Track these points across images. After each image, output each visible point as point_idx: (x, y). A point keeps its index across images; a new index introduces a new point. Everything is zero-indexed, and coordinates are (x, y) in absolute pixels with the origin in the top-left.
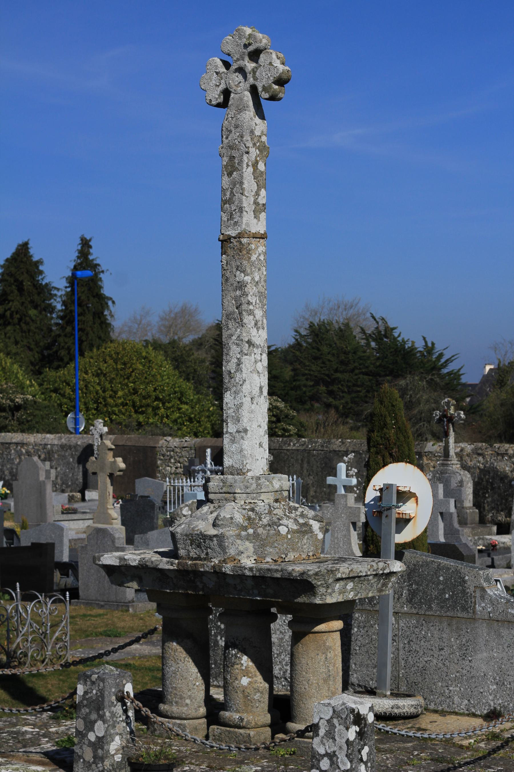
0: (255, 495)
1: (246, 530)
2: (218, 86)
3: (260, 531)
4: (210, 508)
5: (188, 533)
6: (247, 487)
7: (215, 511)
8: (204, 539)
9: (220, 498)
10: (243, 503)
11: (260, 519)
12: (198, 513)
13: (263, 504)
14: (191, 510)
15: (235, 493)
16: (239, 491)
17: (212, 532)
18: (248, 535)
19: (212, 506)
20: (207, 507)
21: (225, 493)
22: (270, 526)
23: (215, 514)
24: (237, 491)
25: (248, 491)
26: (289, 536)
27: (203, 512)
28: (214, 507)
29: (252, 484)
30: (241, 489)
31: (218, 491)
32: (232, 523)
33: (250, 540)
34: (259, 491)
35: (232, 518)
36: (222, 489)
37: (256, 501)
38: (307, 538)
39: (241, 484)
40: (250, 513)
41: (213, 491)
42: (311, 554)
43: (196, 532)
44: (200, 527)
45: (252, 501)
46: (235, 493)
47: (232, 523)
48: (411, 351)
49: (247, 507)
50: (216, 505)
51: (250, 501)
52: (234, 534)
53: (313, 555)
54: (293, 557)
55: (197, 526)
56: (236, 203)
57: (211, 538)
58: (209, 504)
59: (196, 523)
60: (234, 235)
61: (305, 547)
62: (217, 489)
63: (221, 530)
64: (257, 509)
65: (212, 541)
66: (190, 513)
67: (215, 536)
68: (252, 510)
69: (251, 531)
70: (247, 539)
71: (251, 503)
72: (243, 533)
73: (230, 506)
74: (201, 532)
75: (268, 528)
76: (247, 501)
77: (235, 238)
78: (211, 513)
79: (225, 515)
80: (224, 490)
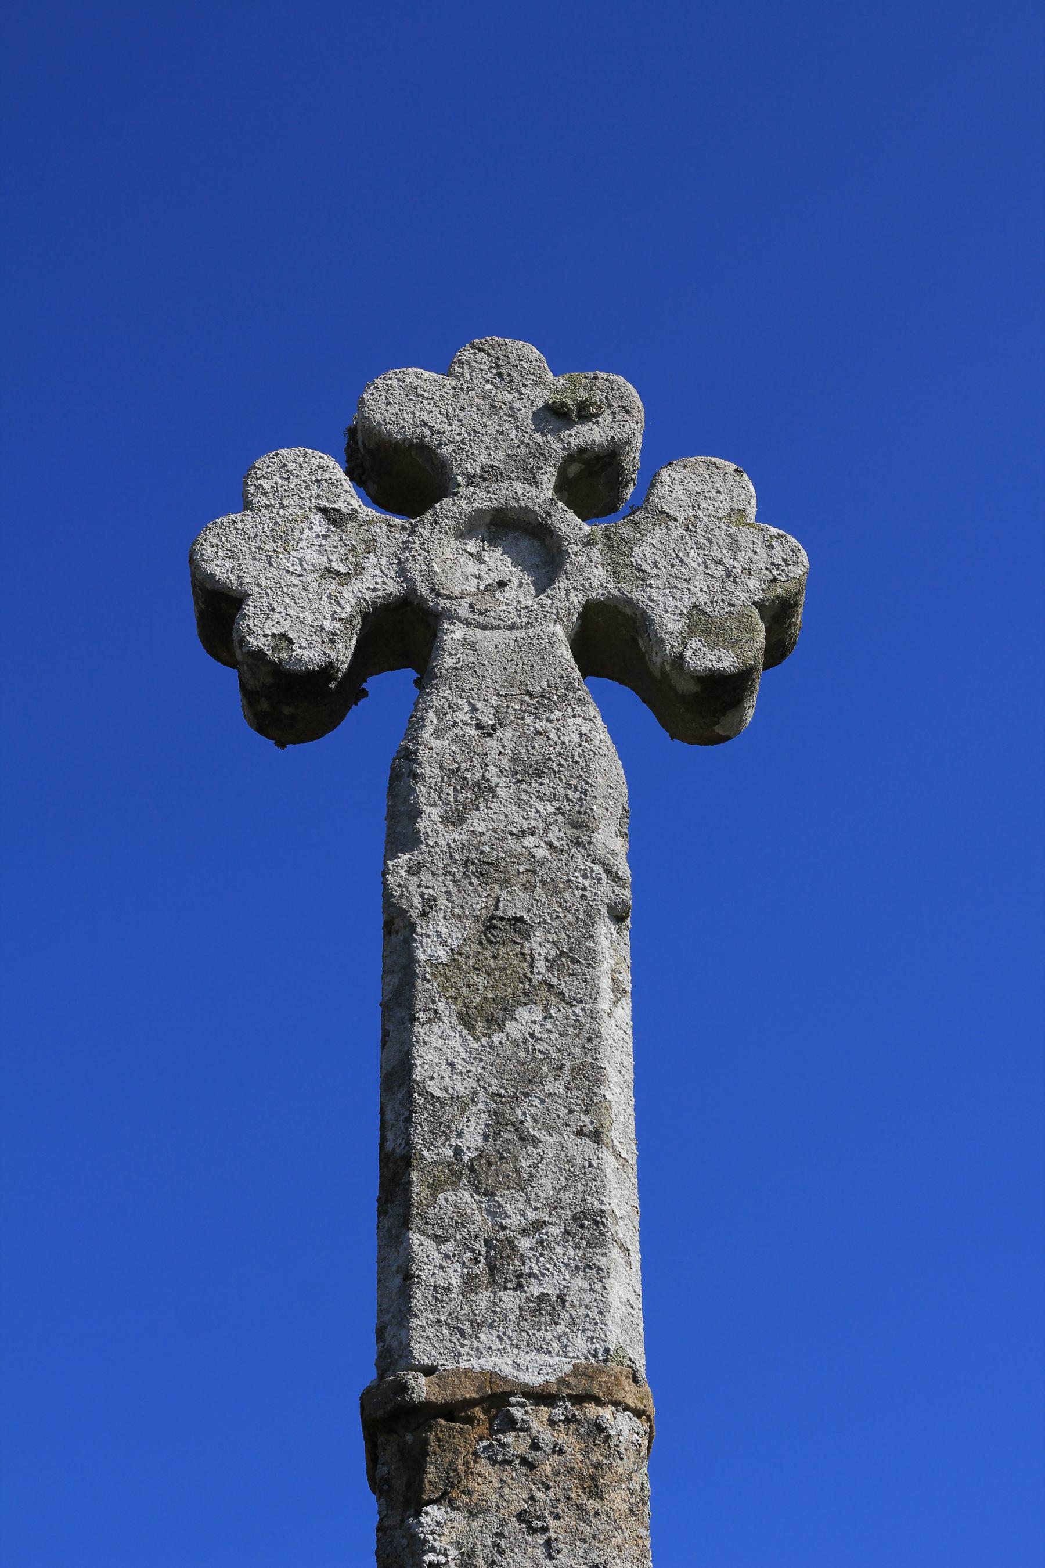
2: (345, 578)
56: (546, 1185)
60: (533, 1379)
77: (542, 1397)
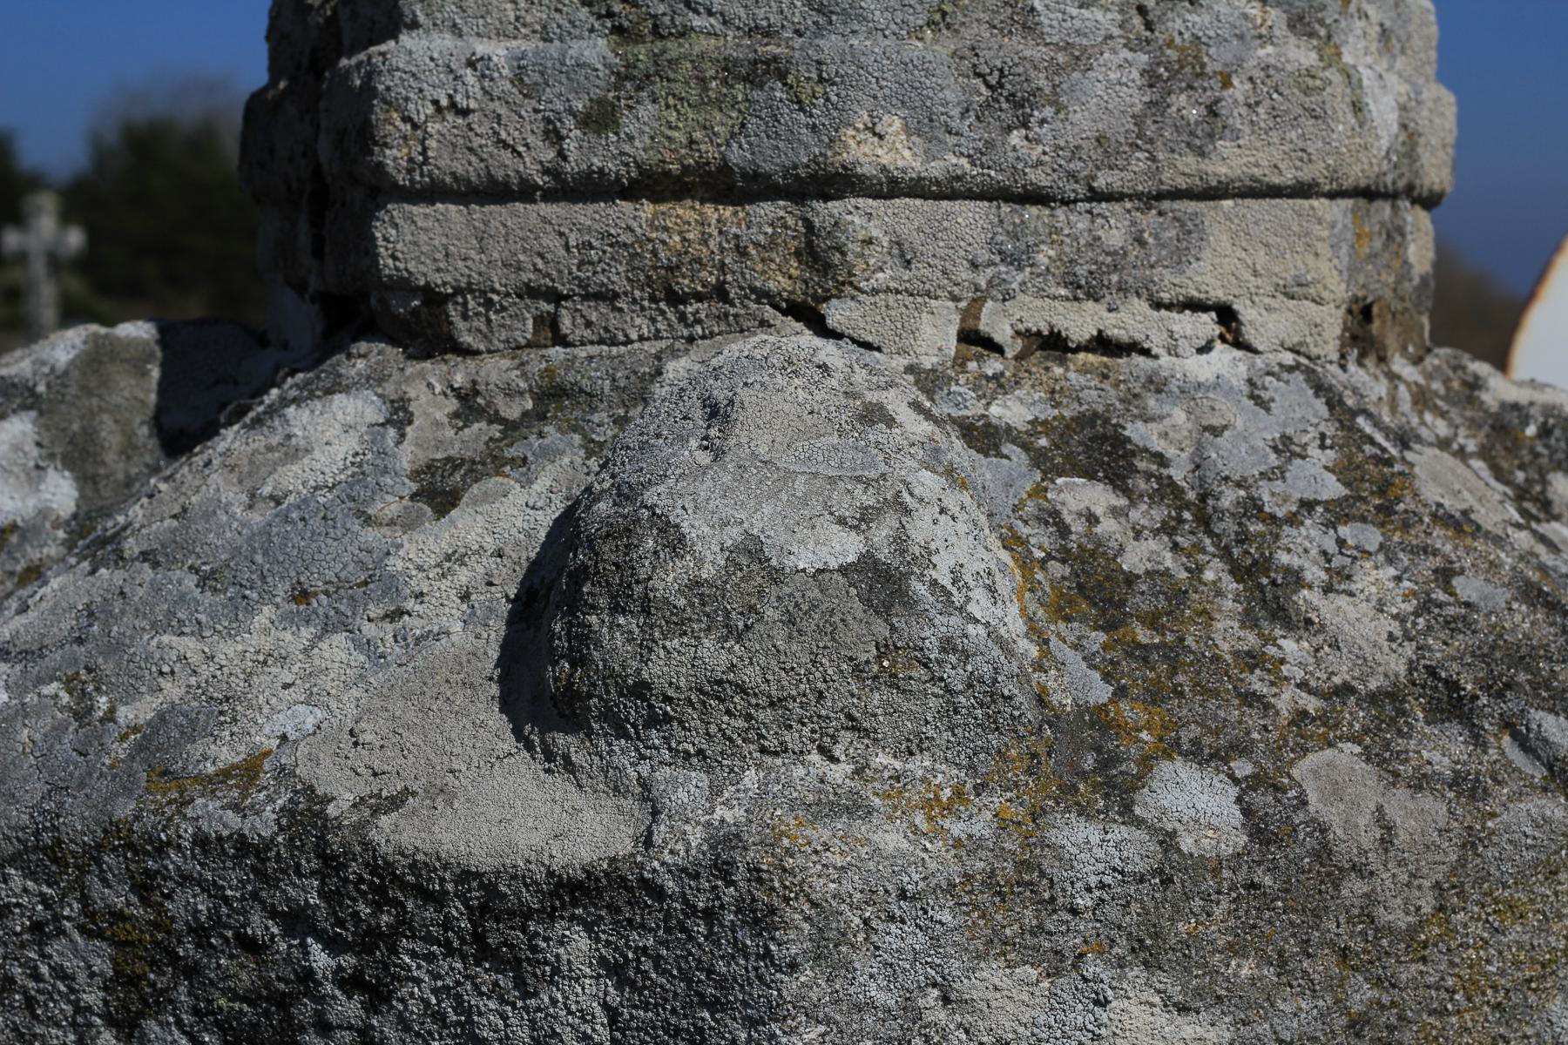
0: (1115, 227)
1: (1118, 793)
3: (1338, 786)
4: (399, 415)
5: (78, 823)
6: (1011, 100)
7: (494, 462)
8: (369, 940)
9: (563, 269)
10: (936, 337)
11: (1272, 600)
12: (222, 482)
13: (1223, 359)
14: (77, 454)
15: (839, 183)
16: (897, 152)
17: (520, 813)
18: (1172, 870)
19: (429, 387)
20: (1162, 294)
21: (651, 185)
22: (1451, 704)
23: (511, 518)
24: (863, 153)
25: (1027, 152)
27: (292, 478)
28: (469, 404)
29: (1080, 59)
30: (926, 126)
31: (535, 159)
32: (892, 666)
33: (1188, 955)
34: (1184, 168)
35: (883, 583)
36: (600, 119)
37: (1133, 319)
39: (937, 49)
40: (1082, 496)
41: (447, 163)
43: (213, 814)
44: (281, 718)
45: (1081, 322)
46: (839, 183)
47: (892, 666)
48: (96, 343)
49: (1012, 411)
50: (495, 370)
51: (1040, 314)
52: (941, 861)
55: (223, 707)
57: (499, 919)
58: (367, 356)
59: (191, 656)
62: (524, 130)
63: (685, 789)
64: (1162, 432)
65: (525, 972)
66: (61, 492)
67: (574, 893)
68: (1100, 450)
69: (1197, 804)
70: (1148, 951)
71: (1054, 344)
72: (1088, 845)
73: (781, 378)
74: (307, 814)
75: (1443, 748)
76: (998, 324)
78: (439, 492)
79: (763, 520)
80: (647, 132)
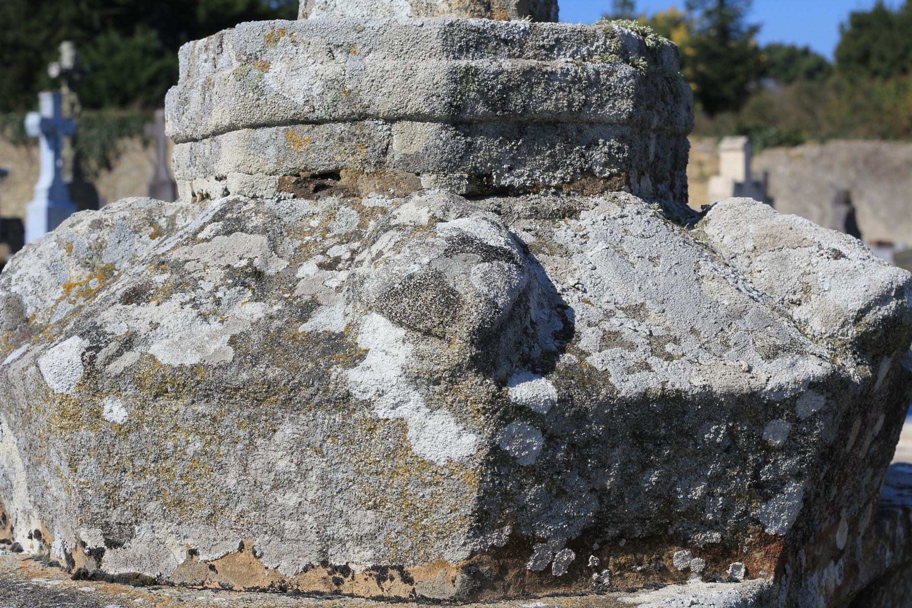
26: (115, 411)
38: (299, 446)
42: (360, 559)
53: (380, 573)
54: (179, 556)
61: (291, 499)
